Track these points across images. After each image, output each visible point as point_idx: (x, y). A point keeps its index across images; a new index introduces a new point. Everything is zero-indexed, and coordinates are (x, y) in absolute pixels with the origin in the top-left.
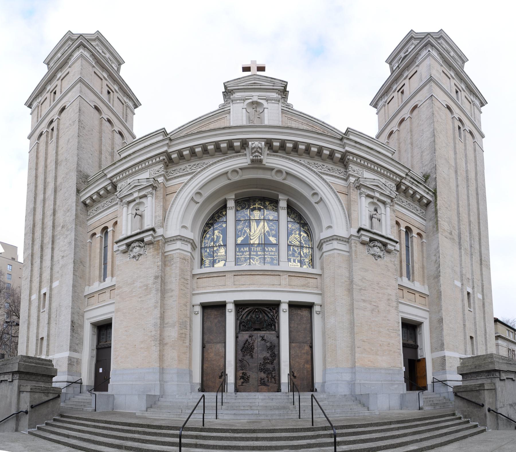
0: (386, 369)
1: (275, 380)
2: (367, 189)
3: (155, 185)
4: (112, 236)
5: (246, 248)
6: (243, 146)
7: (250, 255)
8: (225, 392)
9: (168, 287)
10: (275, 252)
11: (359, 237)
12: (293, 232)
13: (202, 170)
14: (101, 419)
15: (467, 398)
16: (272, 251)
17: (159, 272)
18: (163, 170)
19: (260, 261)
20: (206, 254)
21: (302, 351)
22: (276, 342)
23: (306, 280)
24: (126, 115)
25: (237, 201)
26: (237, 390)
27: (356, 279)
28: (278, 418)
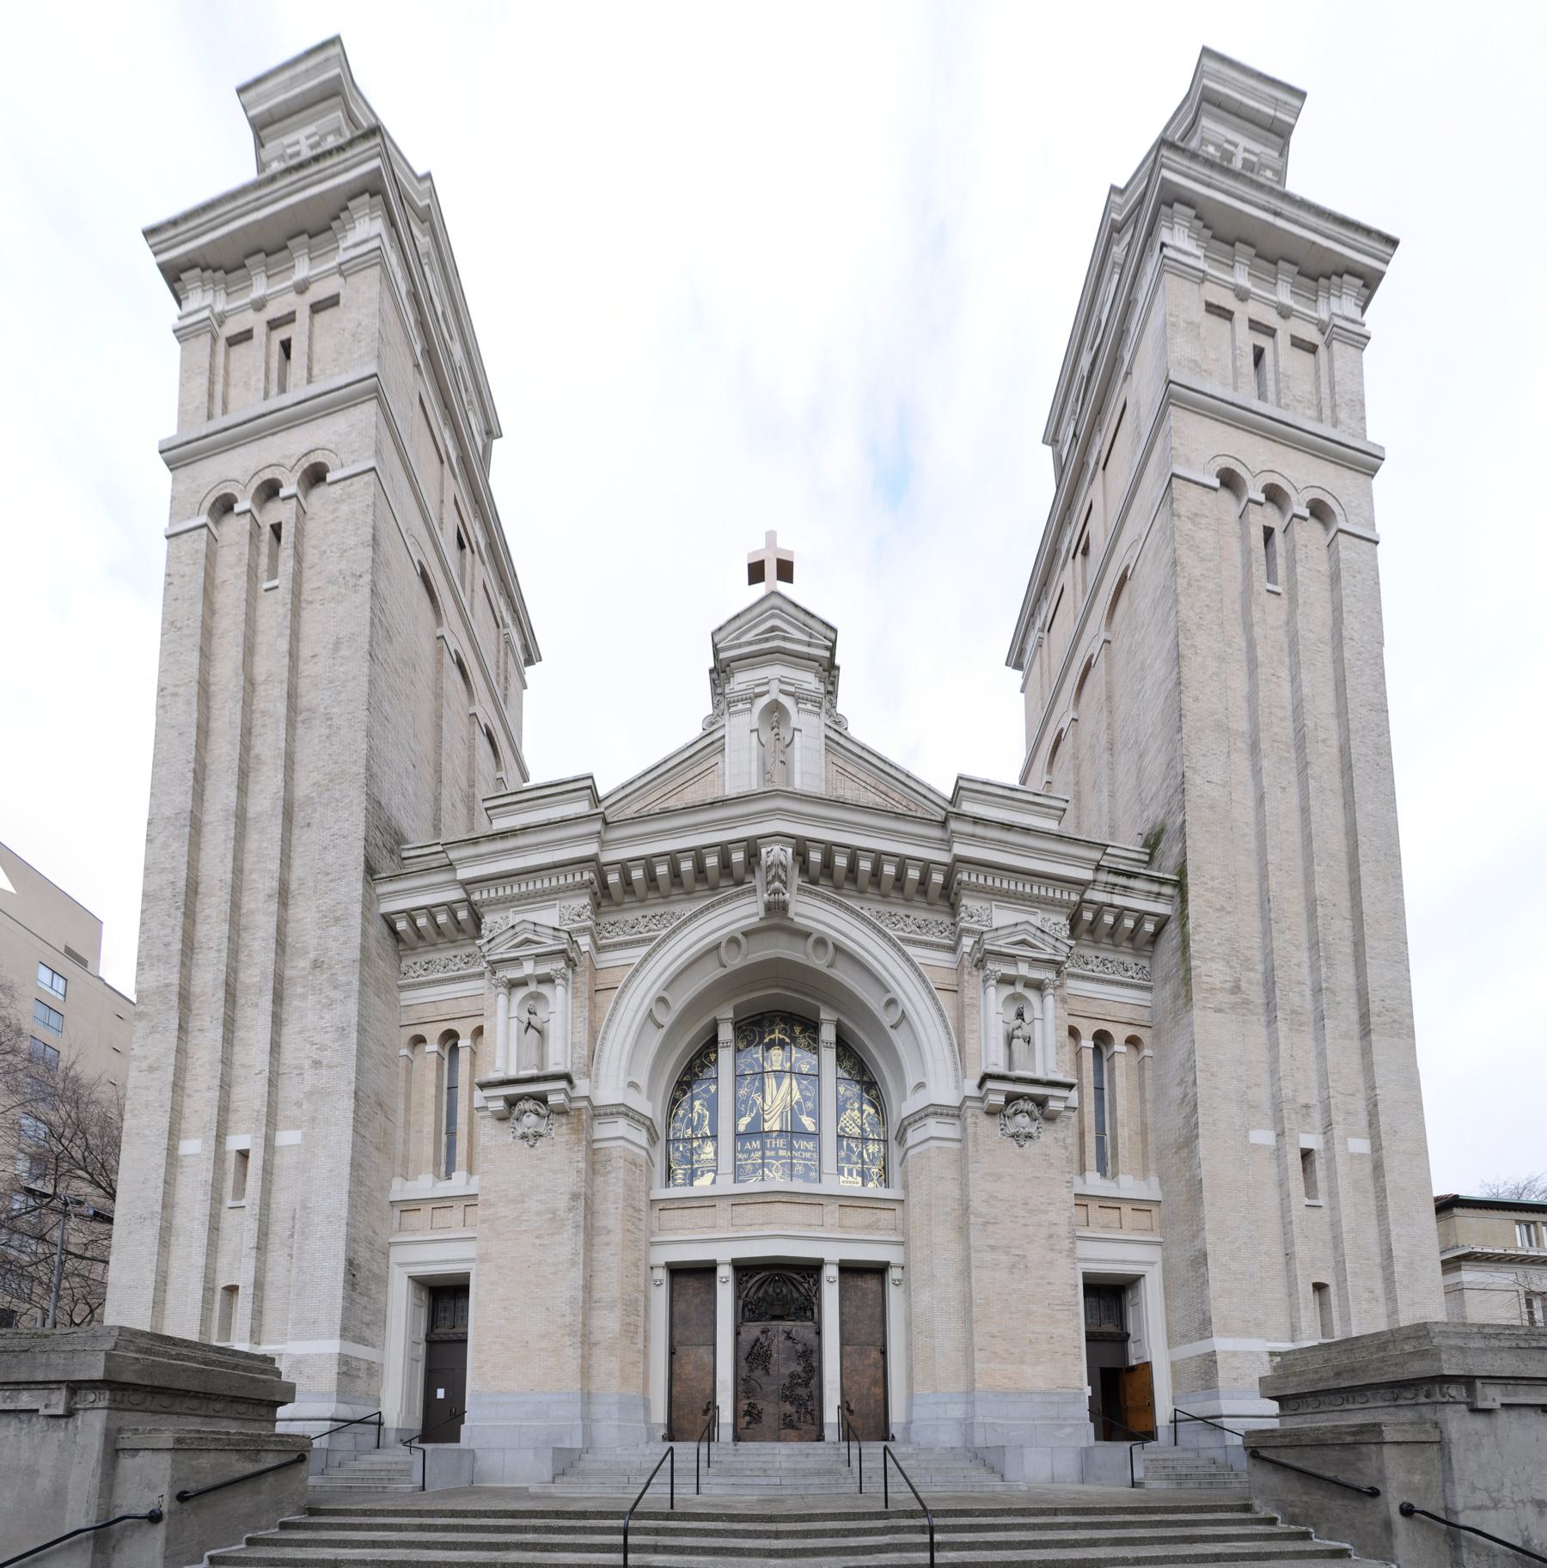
0: (1044, 1393)
1: (813, 1419)
4: (468, 1063)
7: (763, 1158)
8: (713, 1441)
9: (601, 1222)
11: (982, 1099)
12: (848, 1106)
14: (440, 1507)
15: (1299, 1465)
16: (806, 1150)
17: (580, 1184)
19: (784, 1171)
20: (677, 1154)
21: (866, 1362)
22: (815, 1344)
23: (873, 1214)
25: (738, 1025)
26: (737, 1438)
27: (976, 1203)
28: (820, 1492)
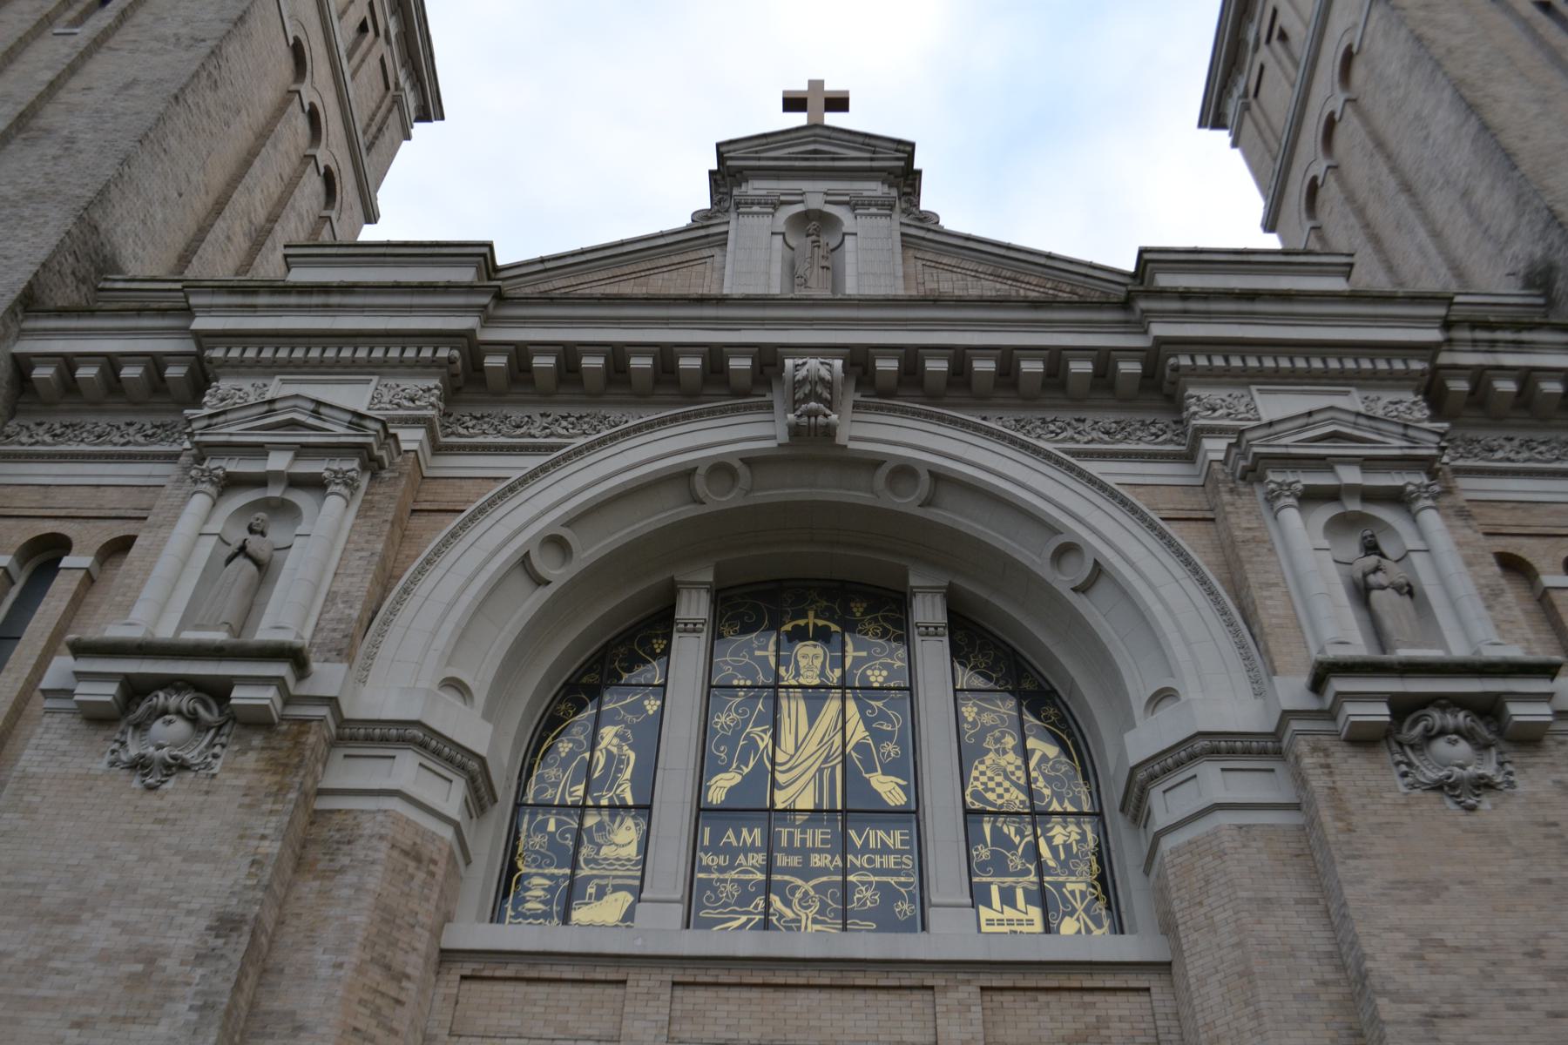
2: (1294, 469)
3: (377, 452)
4: (67, 598)
5: (750, 832)
6: (762, 372)
7: (769, 868)
10: (902, 853)
12: (989, 743)
13: (590, 447)
16: (885, 850)
17: (250, 895)
18: (433, 399)
19: (824, 905)
20: (538, 840)
23: (1085, 1006)
24: (380, 130)
